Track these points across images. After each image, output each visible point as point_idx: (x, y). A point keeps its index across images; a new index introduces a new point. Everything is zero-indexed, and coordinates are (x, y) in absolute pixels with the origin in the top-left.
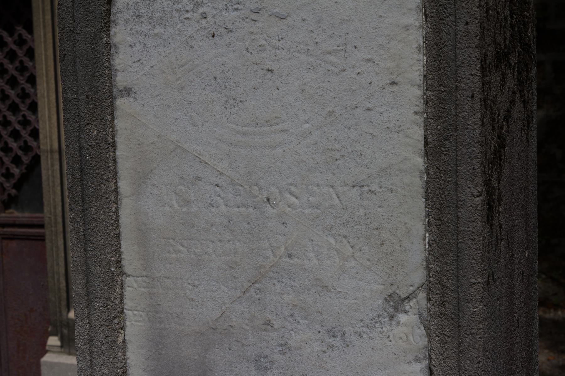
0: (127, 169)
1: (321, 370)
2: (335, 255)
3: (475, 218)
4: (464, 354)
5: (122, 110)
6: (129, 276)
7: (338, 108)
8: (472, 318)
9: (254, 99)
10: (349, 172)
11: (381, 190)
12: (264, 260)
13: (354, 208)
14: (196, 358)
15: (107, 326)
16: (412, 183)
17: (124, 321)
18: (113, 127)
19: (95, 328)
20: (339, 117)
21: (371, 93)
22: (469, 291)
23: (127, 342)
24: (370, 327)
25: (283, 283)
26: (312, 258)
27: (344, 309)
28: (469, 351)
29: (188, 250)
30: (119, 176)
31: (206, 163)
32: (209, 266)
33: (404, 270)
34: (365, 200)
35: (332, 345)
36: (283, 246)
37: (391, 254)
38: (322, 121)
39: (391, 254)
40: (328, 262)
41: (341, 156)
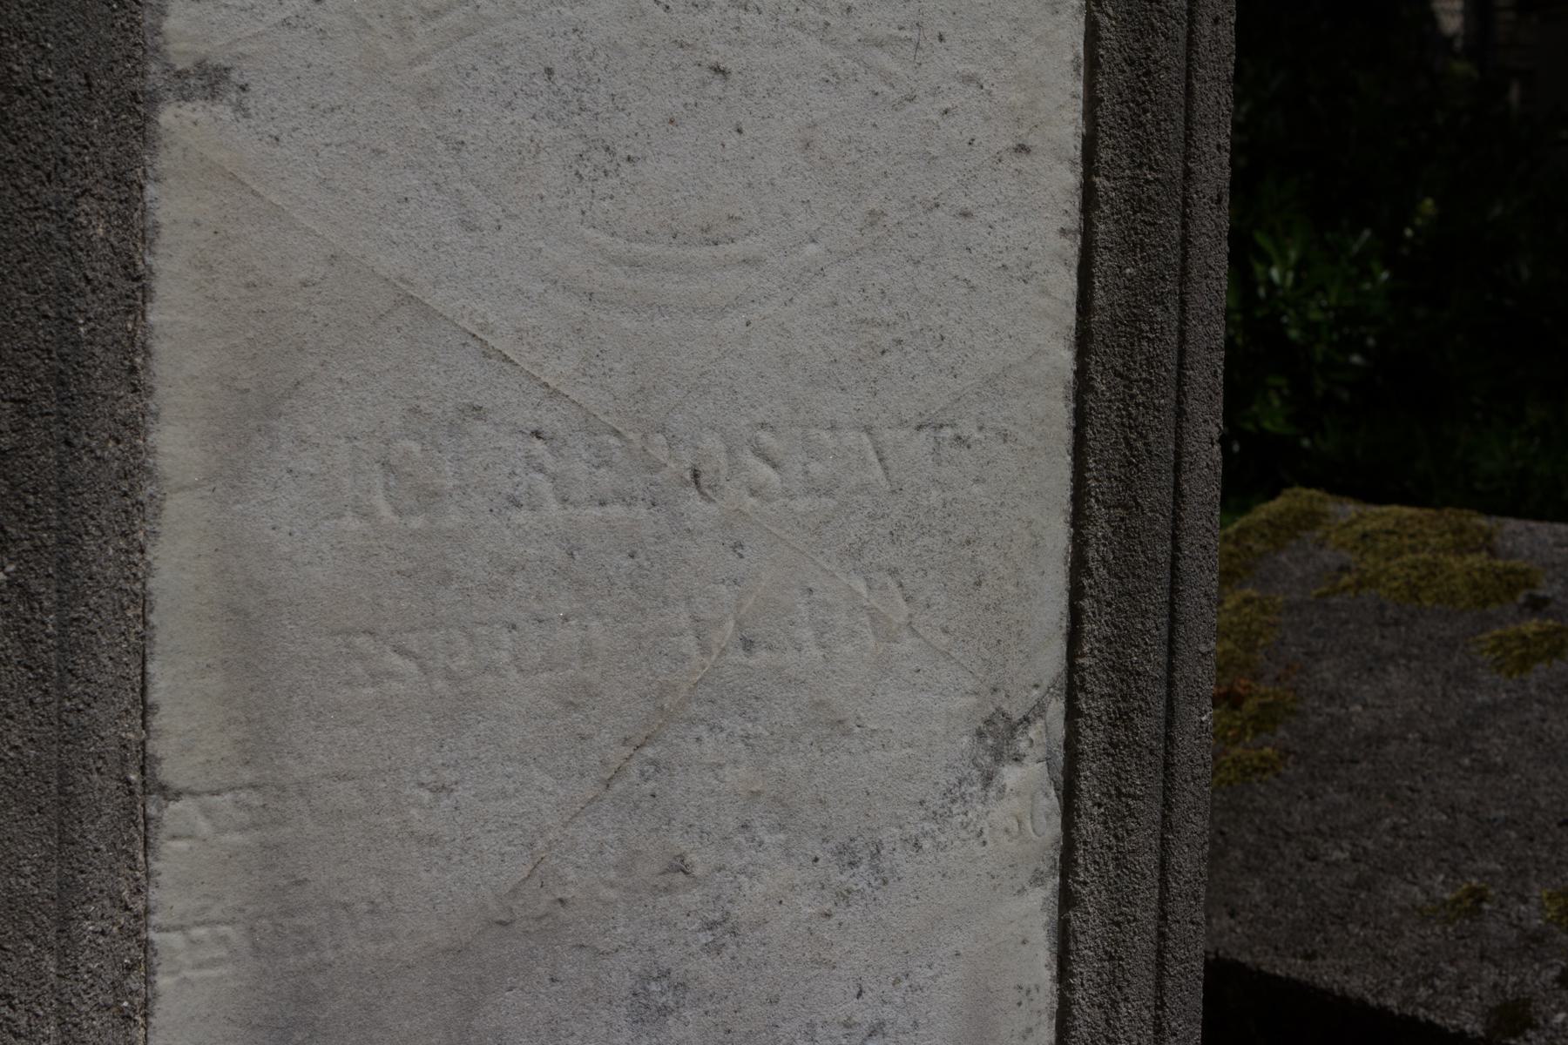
1: (817, 972)
4: (1179, 832)
5: (185, 149)
6: (178, 795)
9: (668, 155)
10: (910, 386)
12: (674, 667)
19: (75, 1025)
20: (894, 229)
22: (1194, 676)
25: (722, 730)
29: (421, 666)
31: (506, 359)
32: (495, 712)
34: (943, 463)
38: (851, 240)
40: (848, 649)
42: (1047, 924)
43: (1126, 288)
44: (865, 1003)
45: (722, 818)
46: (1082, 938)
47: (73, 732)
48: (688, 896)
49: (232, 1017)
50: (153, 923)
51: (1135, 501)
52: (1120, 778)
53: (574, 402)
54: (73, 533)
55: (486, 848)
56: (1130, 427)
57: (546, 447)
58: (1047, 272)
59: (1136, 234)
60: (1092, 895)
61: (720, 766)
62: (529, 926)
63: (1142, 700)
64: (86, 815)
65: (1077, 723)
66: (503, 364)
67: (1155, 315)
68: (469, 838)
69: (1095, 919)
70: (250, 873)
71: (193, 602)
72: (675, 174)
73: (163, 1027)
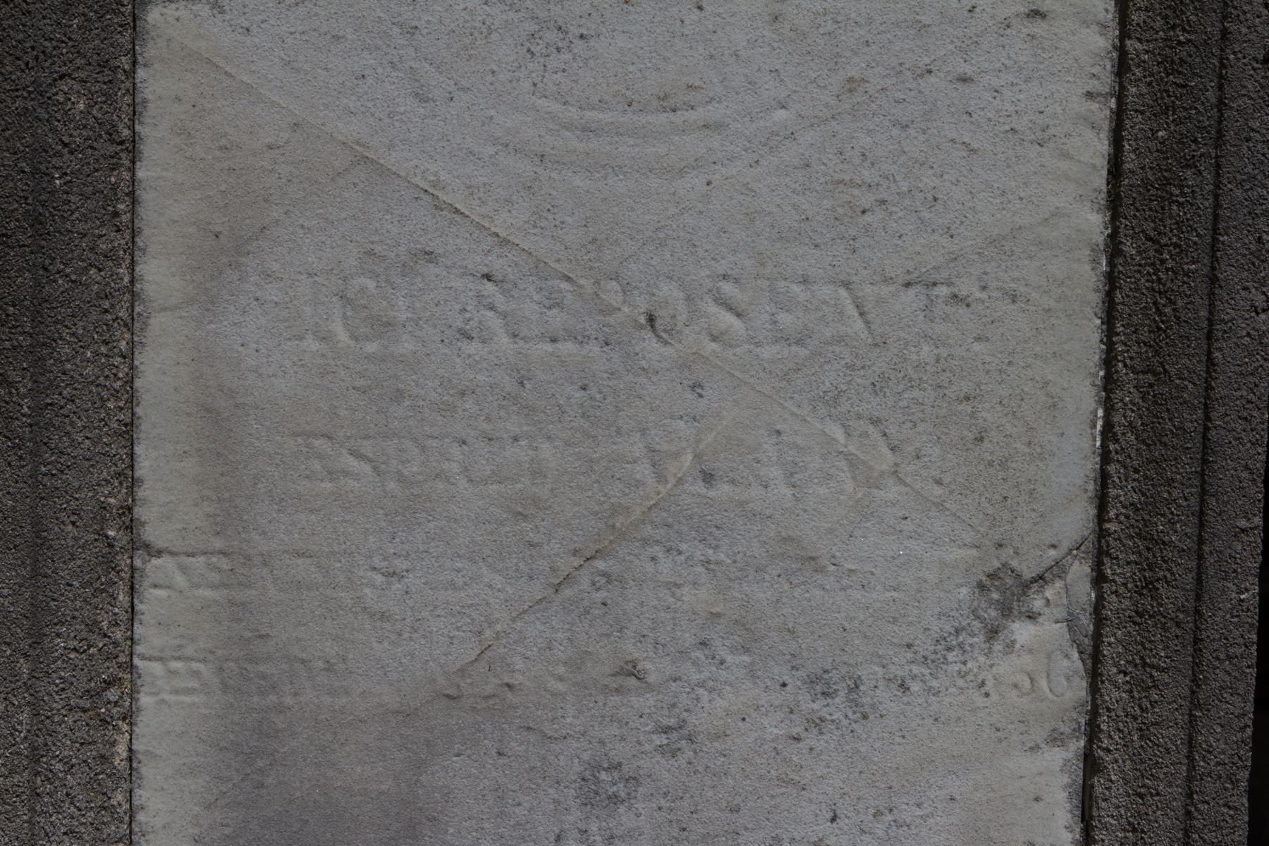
0: (174, 222)
1: (783, 790)
2: (843, 471)
3: (1257, 364)
4: (1208, 710)
5: (168, 41)
6: (159, 553)
7: (876, 70)
8: (1232, 617)
9: (623, 32)
10: (897, 245)
11: (984, 295)
12: (627, 491)
13: (907, 344)
14: (383, 787)
15: (85, 711)
16: (1068, 278)
17: (133, 693)
18: (133, 91)
19: (48, 718)
20: (877, 95)
21: (972, 35)
22: (1229, 551)
23: (140, 757)
24: (933, 661)
25: (680, 553)
26: (777, 482)
27: (862, 617)
28: (1221, 701)
29: (375, 468)
30: (141, 244)
31: (457, 211)
32: (445, 514)
33: (1035, 507)
34: (937, 320)
35: (820, 719)
36: (689, 450)
37: (1003, 465)
38: (826, 105)
39: (1003, 465)
40: (822, 491)
41: (876, 200)
42: (1065, 787)
43: (1158, 151)
44: (840, 829)
45: (679, 633)
46: (1103, 804)
47: (47, 491)
48: (641, 700)
49: (203, 737)
50: (138, 652)
51: (1163, 367)
52: (1145, 648)
53: (524, 250)
54: (49, 338)
55: (435, 629)
56: (1160, 293)
57: (496, 288)
58: (1068, 135)
59: (1169, 96)
60: (1116, 767)
61: (678, 586)
62: (477, 703)
63: (1168, 570)
64: (58, 557)
65: (1103, 587)
66: (455, 216)
67: (1185, 179)
68: (419, 620)
69: (1118, 789)
70: (220, 623)
71: (172, 400)
72: (629, 49)
73: (144, 736)
